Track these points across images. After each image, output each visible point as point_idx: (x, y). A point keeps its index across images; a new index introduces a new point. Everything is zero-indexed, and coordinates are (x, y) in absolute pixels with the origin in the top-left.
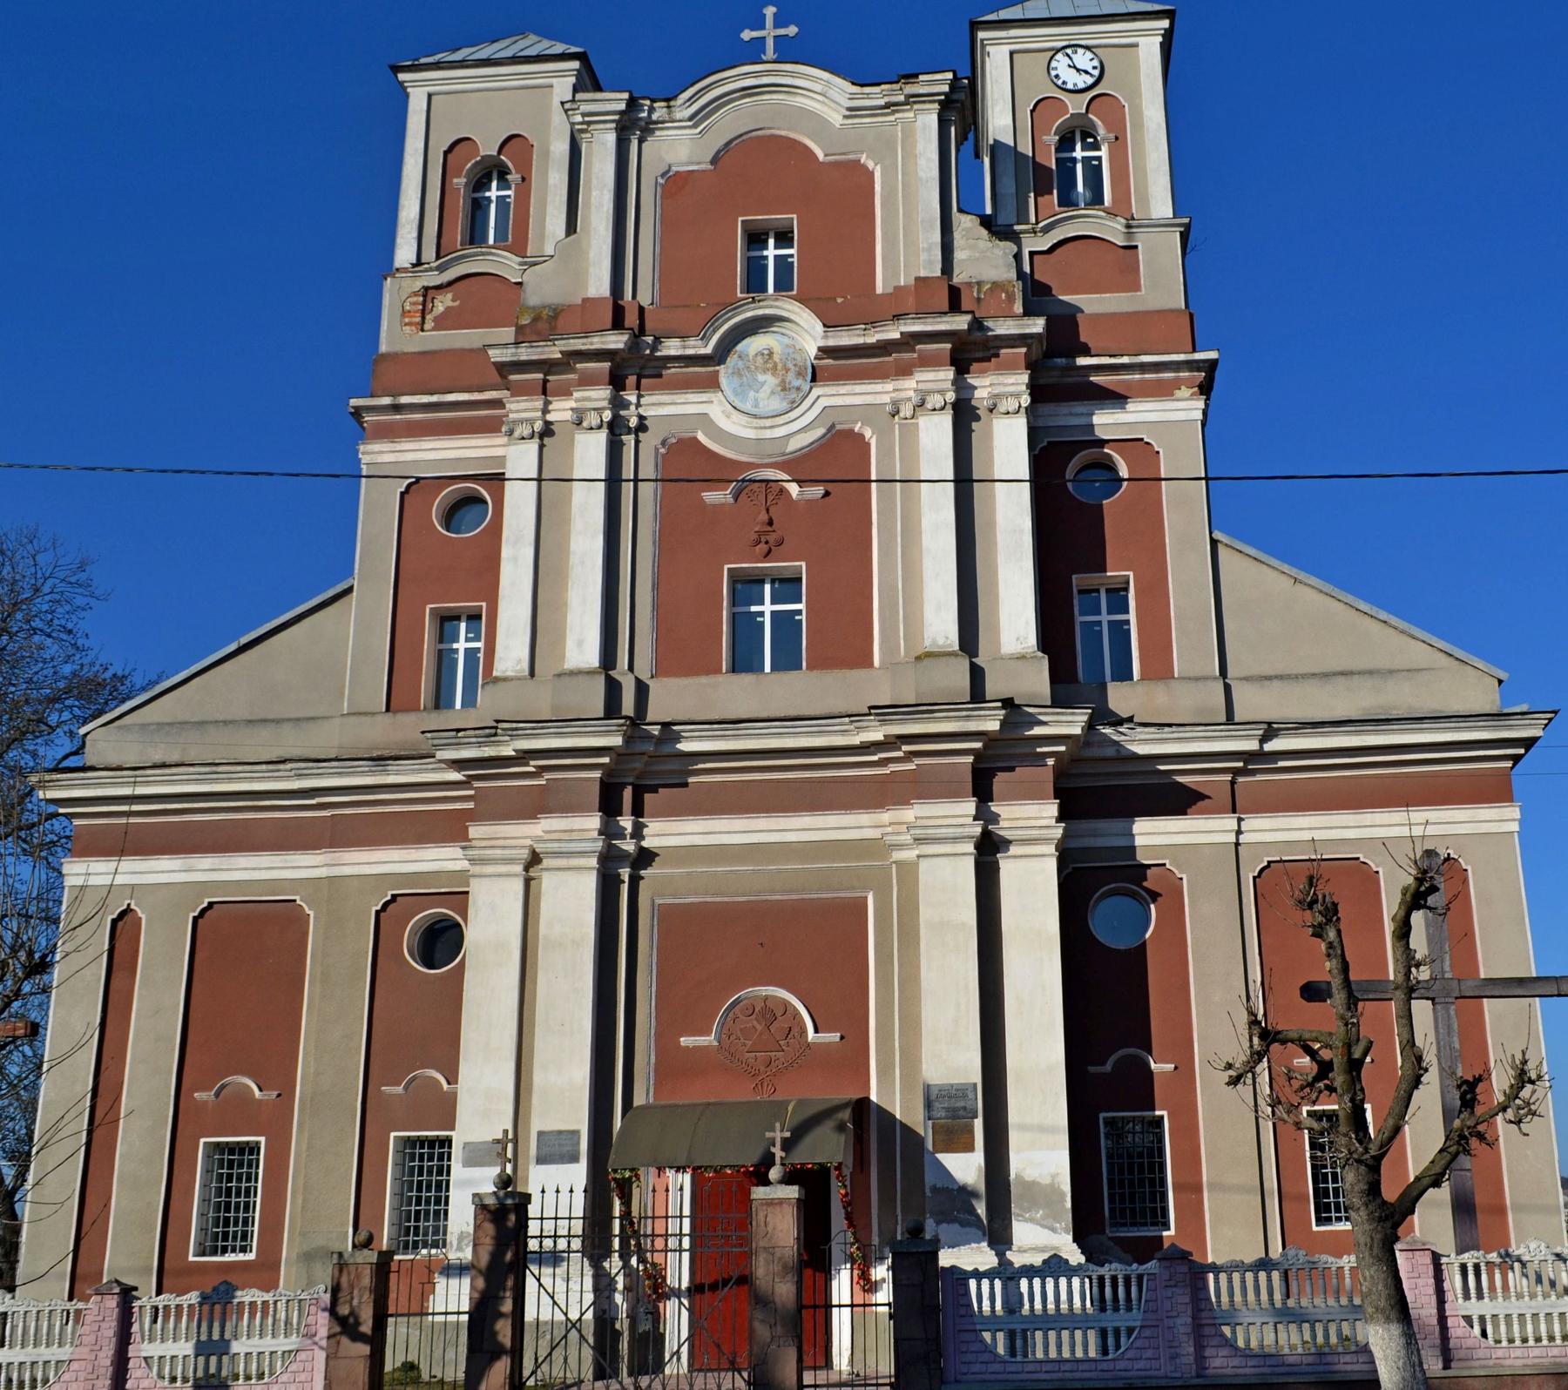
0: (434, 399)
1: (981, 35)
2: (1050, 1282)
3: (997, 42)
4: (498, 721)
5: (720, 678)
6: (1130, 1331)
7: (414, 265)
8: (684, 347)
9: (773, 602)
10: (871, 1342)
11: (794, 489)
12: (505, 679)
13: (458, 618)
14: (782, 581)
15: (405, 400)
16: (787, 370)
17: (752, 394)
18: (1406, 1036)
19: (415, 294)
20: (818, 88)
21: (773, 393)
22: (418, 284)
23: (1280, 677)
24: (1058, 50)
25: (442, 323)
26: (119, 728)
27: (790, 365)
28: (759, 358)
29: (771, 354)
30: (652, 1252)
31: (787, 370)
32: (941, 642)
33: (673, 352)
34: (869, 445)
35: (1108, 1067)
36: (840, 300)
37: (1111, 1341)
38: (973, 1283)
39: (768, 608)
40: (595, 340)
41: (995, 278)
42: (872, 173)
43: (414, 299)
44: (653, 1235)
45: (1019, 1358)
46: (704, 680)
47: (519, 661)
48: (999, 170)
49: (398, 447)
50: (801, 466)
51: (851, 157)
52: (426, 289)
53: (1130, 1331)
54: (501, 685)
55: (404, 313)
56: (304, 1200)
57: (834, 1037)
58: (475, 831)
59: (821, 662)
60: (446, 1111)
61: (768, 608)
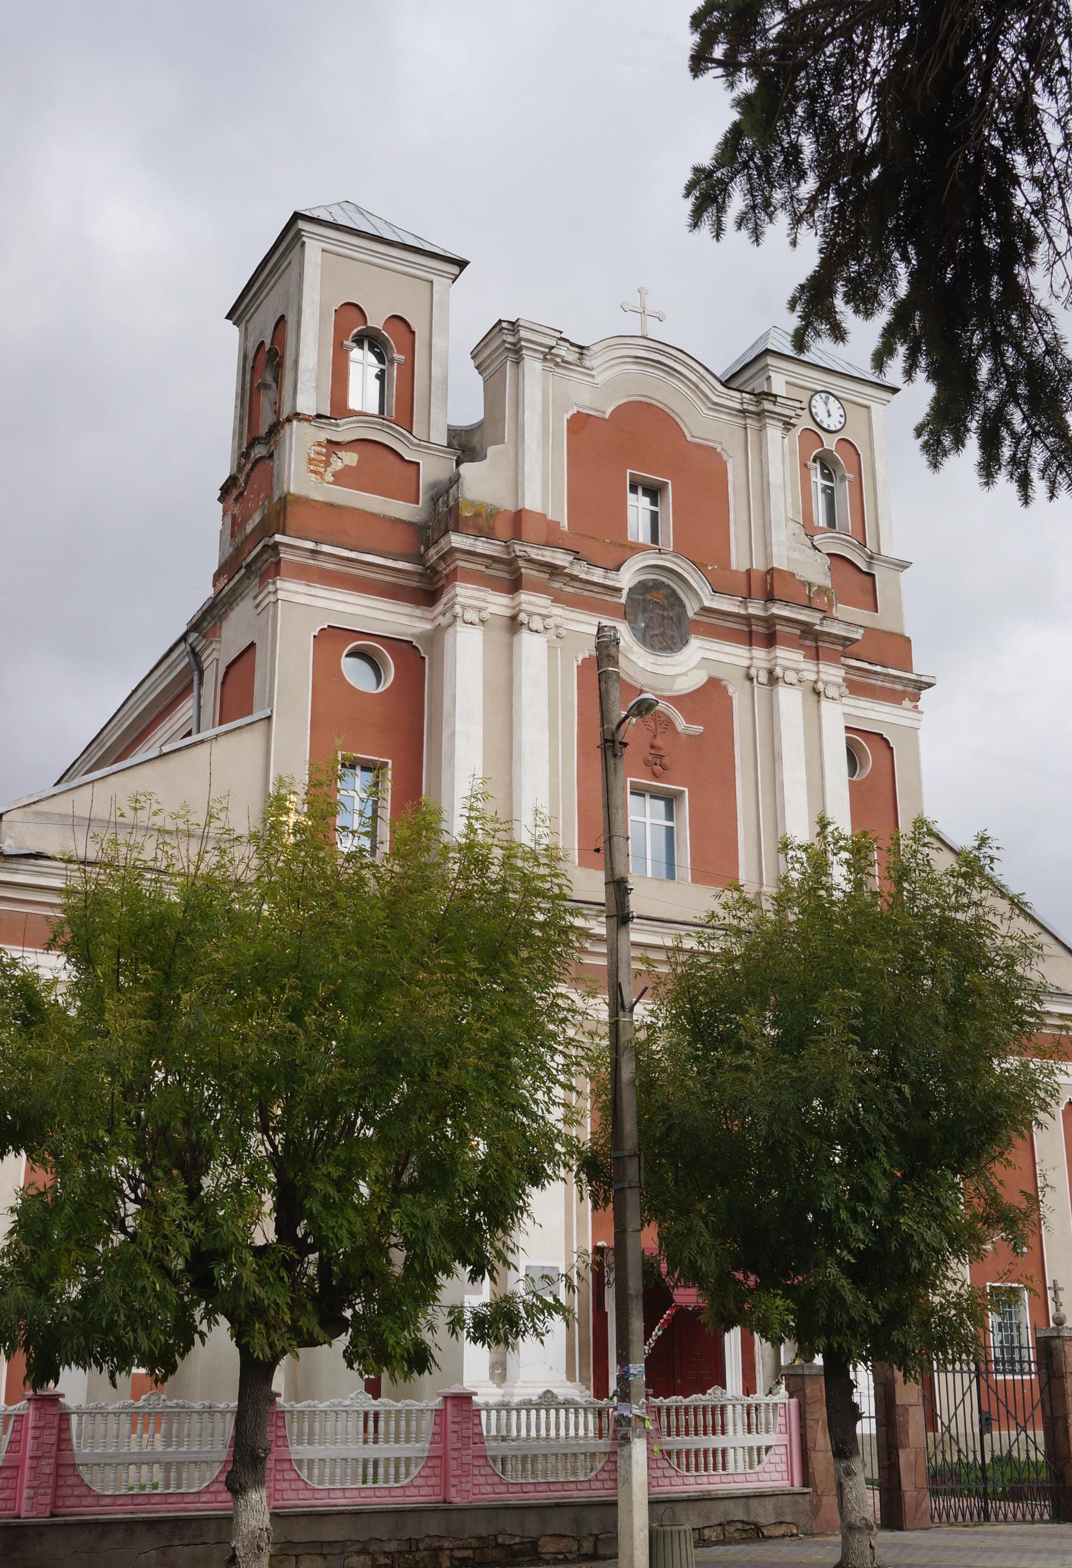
0: (353, 555)
1: (301, 224)
2: (543, 1412)
3: (779, 370)
6: (768, 1449)
10: (868, 1448)
11: (681, 723)
15: (325, 548)
19: (319, 444)
20: (693, 378)
22: (323, 436)
24: (817, 392)
25: (339, 478)
26: (38, 814)
37: (403, 1470)
38: (484, 1414)
40: (547, 553)
43: (318, 449)
45: (370, 1484)
49: (313, 591)
50: (685, 702)
51: (711, 444)
52: (329, 442)
53: (768, 1449)
55: (311, 460)
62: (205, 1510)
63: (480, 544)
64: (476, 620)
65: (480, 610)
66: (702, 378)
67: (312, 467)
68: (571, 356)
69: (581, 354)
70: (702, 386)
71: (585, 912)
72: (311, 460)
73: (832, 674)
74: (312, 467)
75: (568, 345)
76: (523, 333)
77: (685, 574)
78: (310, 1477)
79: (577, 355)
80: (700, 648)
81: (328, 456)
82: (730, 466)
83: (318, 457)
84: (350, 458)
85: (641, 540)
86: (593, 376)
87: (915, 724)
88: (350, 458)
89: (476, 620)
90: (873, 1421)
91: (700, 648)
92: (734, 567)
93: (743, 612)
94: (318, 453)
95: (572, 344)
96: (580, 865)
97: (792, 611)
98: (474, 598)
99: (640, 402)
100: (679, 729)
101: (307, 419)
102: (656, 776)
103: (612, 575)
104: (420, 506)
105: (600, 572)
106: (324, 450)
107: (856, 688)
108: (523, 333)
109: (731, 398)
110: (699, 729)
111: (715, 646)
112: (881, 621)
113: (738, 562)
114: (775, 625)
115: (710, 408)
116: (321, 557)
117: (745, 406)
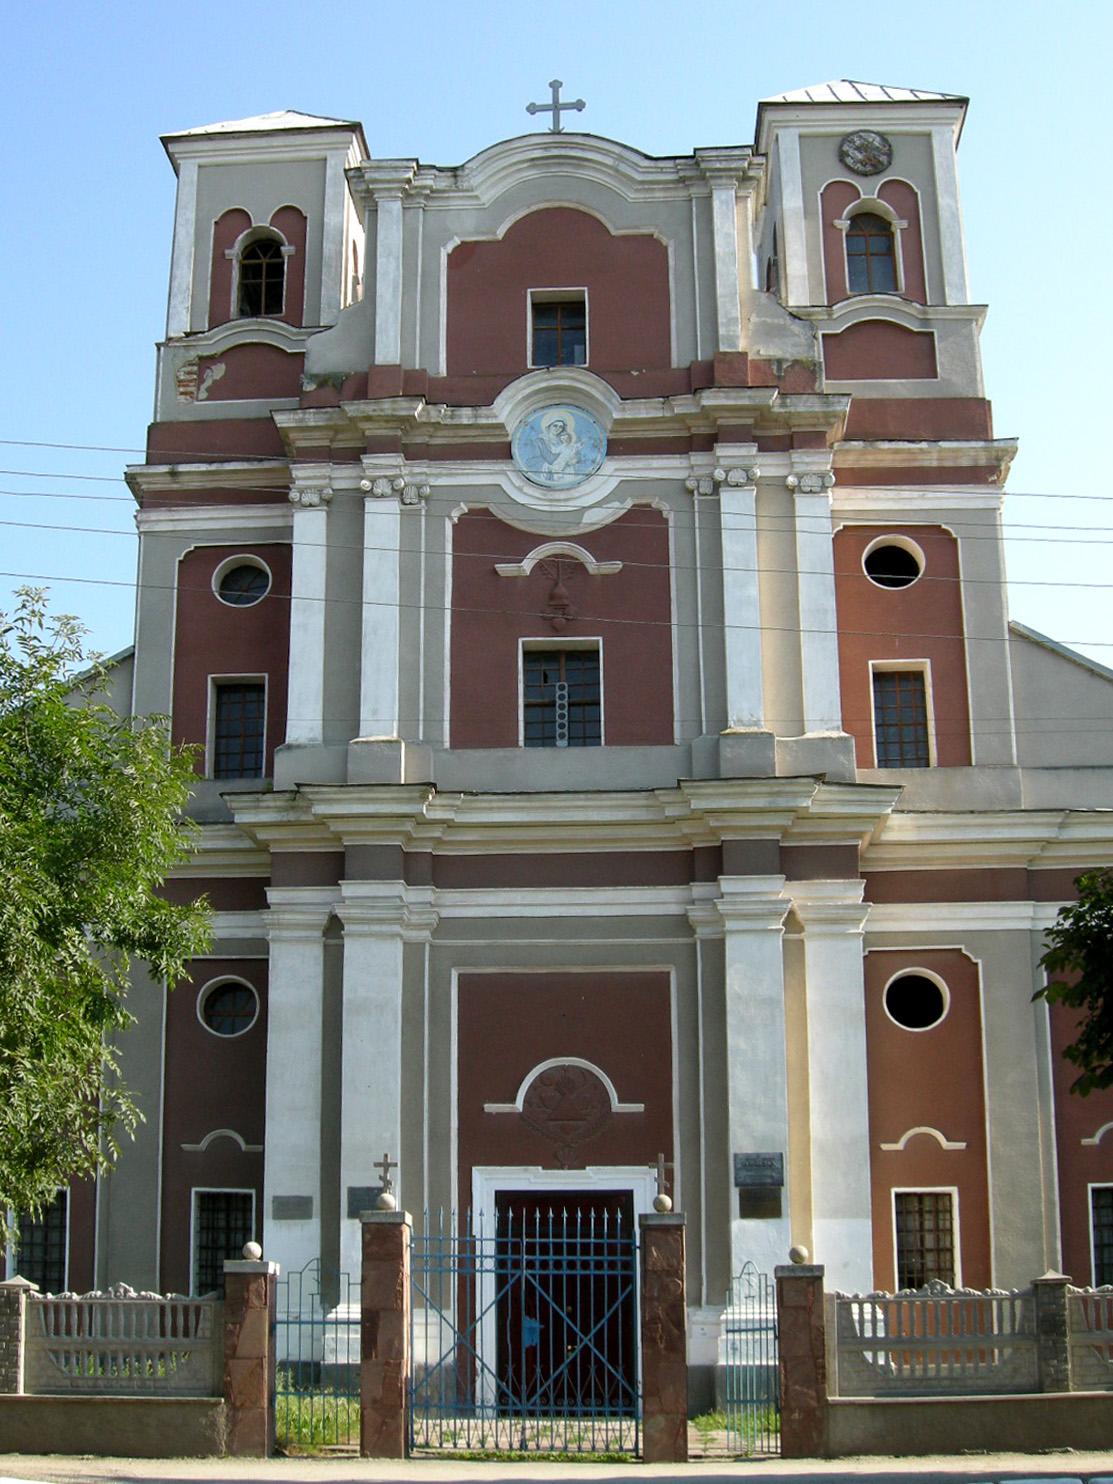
4: (298, 785)
5: (517, 751)
12: (299, 747)
18: (768, 253)
20: (609, 161)
22: (193, 354)
23: (1093, 767)
25: (215, 393)
30: (482, 1272)
33: (465, 421)
36: (635, 373)
41: (234, 1384)
42: (666, 248)
43: (189, 369)
44: (482, 1256)
46: (500, 753)
48: (943, 953)
50: (600, 540)
52: (201, 358)
54: (295, 753)
57: (639, 1107)
58: (273, 895)
59: (622, 737)
60: (253, 1169)
65: (320, 490)
66: (620, 158)
67: (182, 389)
68: (444, 182)
69: (455, 176)
70: (623, 168)
71: (310, 797)
72: (180, 383)
74: (182, 389)
75: (434, 172)
77: (587, 388)
79: (452, 180)
82: (671, 251)
83: (188, 377)
84: (218, 371)
85: (388, 351)
86: (476, 197)
87: (992, 504)
88: (218, 371)
89: (315, 499)
92: (674, 365)
93: (668, 414)
94: (189, 373)
95: (440, 170)
97: (727, 398)
98: (315, 478)
99: (548, 209)
100: (591, 571)
101: (180, 339)
102: (556, 632)
103: (483, 411)
106: (195, 368)
107: (851, 478)
109: (662, 171)
110: (618, 565)
112: (948, 379)
114: (715, 420)
115: (637, 190)
117: (682, 174)
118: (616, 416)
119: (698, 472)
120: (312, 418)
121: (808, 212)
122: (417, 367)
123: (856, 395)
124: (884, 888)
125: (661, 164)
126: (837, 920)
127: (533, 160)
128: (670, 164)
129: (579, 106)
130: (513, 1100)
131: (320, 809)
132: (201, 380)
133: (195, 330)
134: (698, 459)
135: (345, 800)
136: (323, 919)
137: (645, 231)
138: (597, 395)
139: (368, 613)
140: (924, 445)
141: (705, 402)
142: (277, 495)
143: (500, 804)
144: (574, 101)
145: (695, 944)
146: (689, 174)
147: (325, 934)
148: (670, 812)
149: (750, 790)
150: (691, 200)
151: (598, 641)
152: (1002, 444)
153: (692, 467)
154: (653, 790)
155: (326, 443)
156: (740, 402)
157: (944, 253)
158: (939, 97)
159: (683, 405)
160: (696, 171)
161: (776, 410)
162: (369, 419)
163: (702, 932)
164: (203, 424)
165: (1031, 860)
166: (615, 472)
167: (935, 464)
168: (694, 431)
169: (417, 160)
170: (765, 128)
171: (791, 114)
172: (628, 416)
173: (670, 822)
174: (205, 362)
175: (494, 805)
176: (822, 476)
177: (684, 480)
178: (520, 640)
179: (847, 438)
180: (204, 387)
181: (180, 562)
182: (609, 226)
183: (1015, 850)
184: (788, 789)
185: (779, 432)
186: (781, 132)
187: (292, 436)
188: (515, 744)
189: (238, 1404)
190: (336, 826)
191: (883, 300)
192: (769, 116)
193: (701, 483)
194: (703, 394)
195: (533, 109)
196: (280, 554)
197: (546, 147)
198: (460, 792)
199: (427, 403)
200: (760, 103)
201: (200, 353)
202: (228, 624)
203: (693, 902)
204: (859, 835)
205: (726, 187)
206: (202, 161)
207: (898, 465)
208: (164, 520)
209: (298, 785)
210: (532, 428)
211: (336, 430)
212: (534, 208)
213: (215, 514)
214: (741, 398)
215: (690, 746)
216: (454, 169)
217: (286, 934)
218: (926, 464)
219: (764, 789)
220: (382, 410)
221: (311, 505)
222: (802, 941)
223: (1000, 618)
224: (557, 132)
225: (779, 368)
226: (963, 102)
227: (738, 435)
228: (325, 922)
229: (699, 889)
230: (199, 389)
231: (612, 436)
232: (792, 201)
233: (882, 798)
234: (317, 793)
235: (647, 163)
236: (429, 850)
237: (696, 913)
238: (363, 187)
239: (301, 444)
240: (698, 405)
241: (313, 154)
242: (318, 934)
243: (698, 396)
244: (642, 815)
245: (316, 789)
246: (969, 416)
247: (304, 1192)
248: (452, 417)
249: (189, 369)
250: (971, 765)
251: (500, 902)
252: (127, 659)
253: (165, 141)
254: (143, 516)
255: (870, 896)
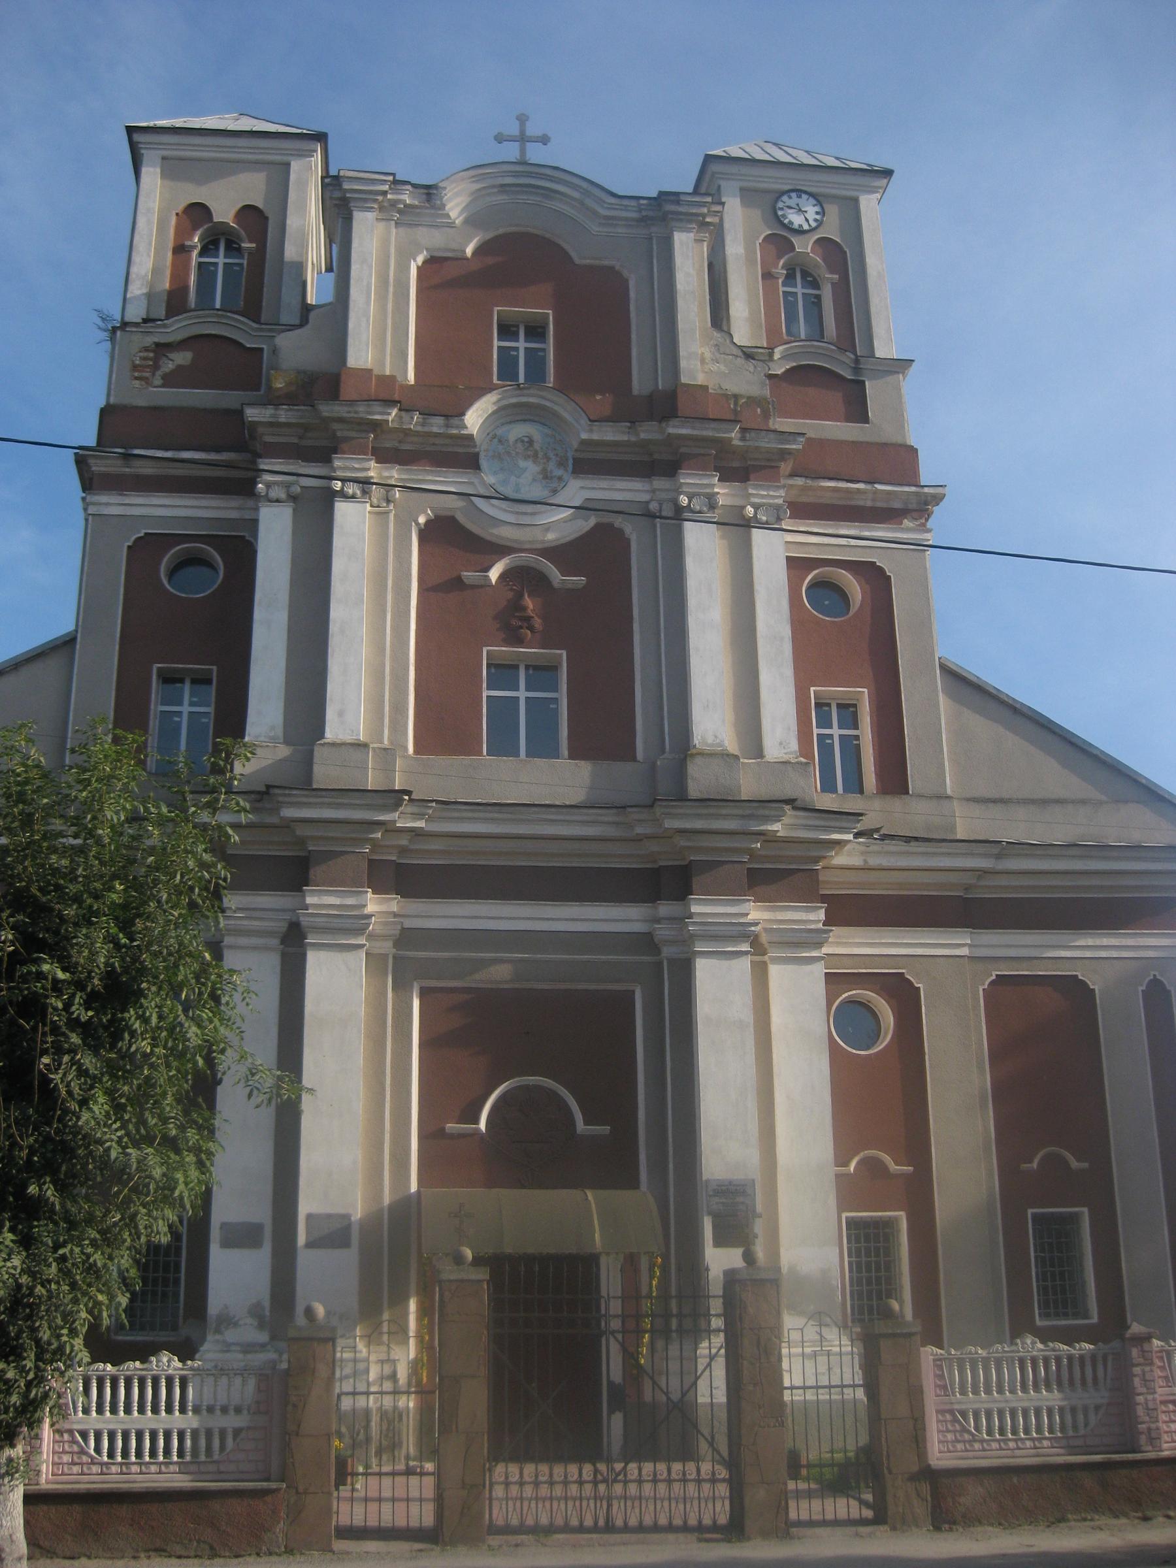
0: (169, 454)
7: (145, 321)
8: (447, 426)
9: (527, 690)
13: (182, 681)
14: (536, 668)
16: (548, 459)
17: (513, 478)
19: (146, 349)
21: (534, 480)
22: (150, 340)
25: (170, 380)
27: (551, 455)
28: (519, 445)
29: (531, 442)
31: (548, 459)
32: (710, 741)
33: (435, 430)
34: (628, 541)
35: (1035, 1165)
39: (186, 709)
42: (627, 281)
43: (145, 354)
47: (273, 728)
52: (157, 345)
55: (135, 367)
56: (472, 1281)
57: (605, 1129)
61: (186, 709)
62: (1049, 1456)
63: (282, 412)
64: (283, 496)
70: (589, 202)
71: (281, 799)
72: (135, 367)
73: (763, 496)
74: (136, 374)
75: (409, 187)
76: (346, 186)
78: (977, 1428)
80: (582, 488)
81: (156, 360)
82: (632, 284)
83: (144, 363)
84: (182, 358)
88: (182, 358)
89: (283, 496)
90: (787, 1383)
91: (582, 488)
92: (635, 391)
93: (633, 439)
94: (145, 359)
96: (823, 790)
97: (693, 428)
101: (136, 325)
104: (262, 392)
105: (439, 420)
106: (151, 355)
107: (803, 510)
108: (346, 186)
111: (604, 484)
112: (879, 428)
113: (639, 384)
116: (138, 463)
117: (644, 213)
118: (584, 436)
119: (663, 495)
120: (284, 415)
121: (750, 260)
122: (388, 373)
123: (811, 434)
124: (849, 910)
125: (625, 202)
126: (798, 943)
127: (502, 186)
128: (633, 203)
129: (544, 140)
130: (476, 1121)
131: (289, 813)
132: (156, 367)
133: (152, 316)
134: (659, 483)
135: (316, 804)
136: (283, 926)
137: (606, 263)
138: (566, 415)
139: (337, 612)
140: (861, 486)
141: (671, 430)
142: (242, 486)
143: (470, 815)
144: (540, 134)
145: (660, 964)
146: (650, 213)
147: (283, 942)
148: (639, 830)
149: (724, 812)
150: (651, 239)
151: (561, 655)
152: (931, 490)
153: (653, 491)
154: (624, 807)
155: (296, 441)
156: (705, 433)
157: (873, 310)
158: (865, 167)
159: (648, 432)
160: (661, 213)
161: (736, 442)
162: (341, 420)
163: (667, 952)
164: (156, 410)
165: (967, 889)
166: (577, 490)
167: (869, 504)
168: (656, 456)
169: (394, 175)
170: (707, 177)
171: (733, 169)
172: (595, 437)
173: (639, 839)
174: (162, 349)
175: (465, 814)
176: (778, 508)
177: (647, 503)
178: (485, 650)
179: (793, 475)
180: (159, 373)
181: (129, 547)
182: (573, 254)
183: (953, 878)
184: (761, 812)
185: (735, 464)
186: (723, 184)
187: (260, 430)
188: (480, 754)
189: (301, 1489)
190: (300, 831)
191: (819, 347)
192: (714, 167)
193: (664, 506)
194: (671, 423)
195: (500, 139)
196: (240, 551)
197: (516, 174)
198: (432, 801)
199: (400, 410)
200: (707, 155)
201: (156, 340)
202: (184, 619)
203: (658, 920)
204: (817, 860)
205: (689, 230)
206: (166, 153)
207: (835, 502)
208: (112, 504)
209: (268, 787)
210: (500, 441)
211: (306, 428)
212: (501, 231)
213: (204, 503)
214: (707, 429)
215: (654, 764)
216: (428, 187)
217: (243, 941)
218: (861, 503)
219: (736, 812)
220: (356, 412)
221: (278, 501)
222: (765, 963)
223: (933, 654)
224: (523, 162)
225: (736, 404)
226: (888, 173)
227: (701, 464)
228: (285, 929)
229: (665, 909)
230: (154, 375)
231: (578, 455)
232: (735, 249)
233: (844, 824)
234: (289, 795)
235: (612, 200)
236: (394, 858)
237: (663, 932)
238: (337, 194)
239: (268, 439)
240: (653, 433)
241: (278, 158)
242: (275, 942)
243: (664, 425)
244: (611, 832)
245: (287, 792)
246: (900, 460)
247: (255, 1219)
248: (423, 425)
249: (145, 354)
250: (908, 793)
251: (466, 914)
252: (67, 643)
253: (130, 130)
254: (89, 499)
255: (831, 920)
